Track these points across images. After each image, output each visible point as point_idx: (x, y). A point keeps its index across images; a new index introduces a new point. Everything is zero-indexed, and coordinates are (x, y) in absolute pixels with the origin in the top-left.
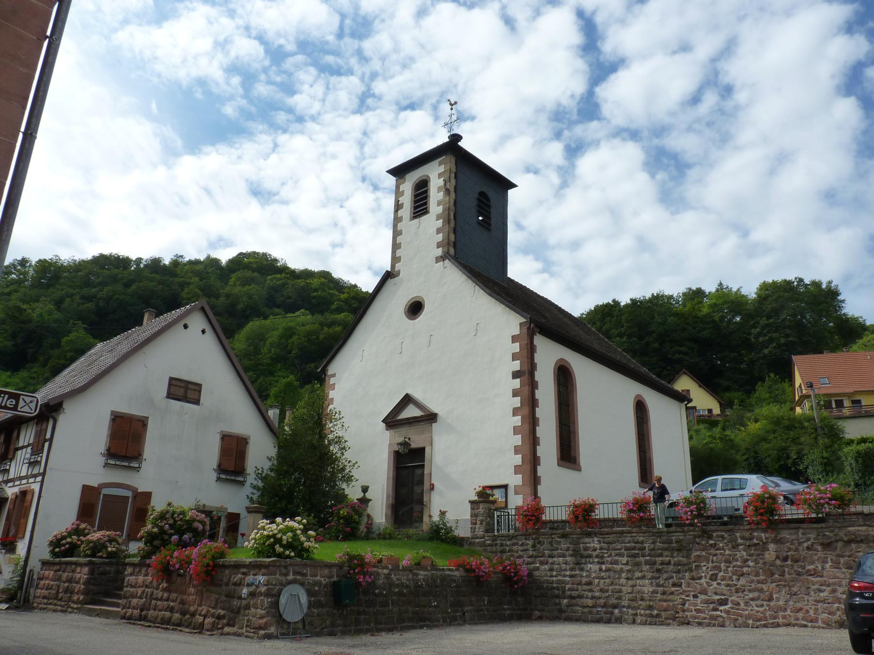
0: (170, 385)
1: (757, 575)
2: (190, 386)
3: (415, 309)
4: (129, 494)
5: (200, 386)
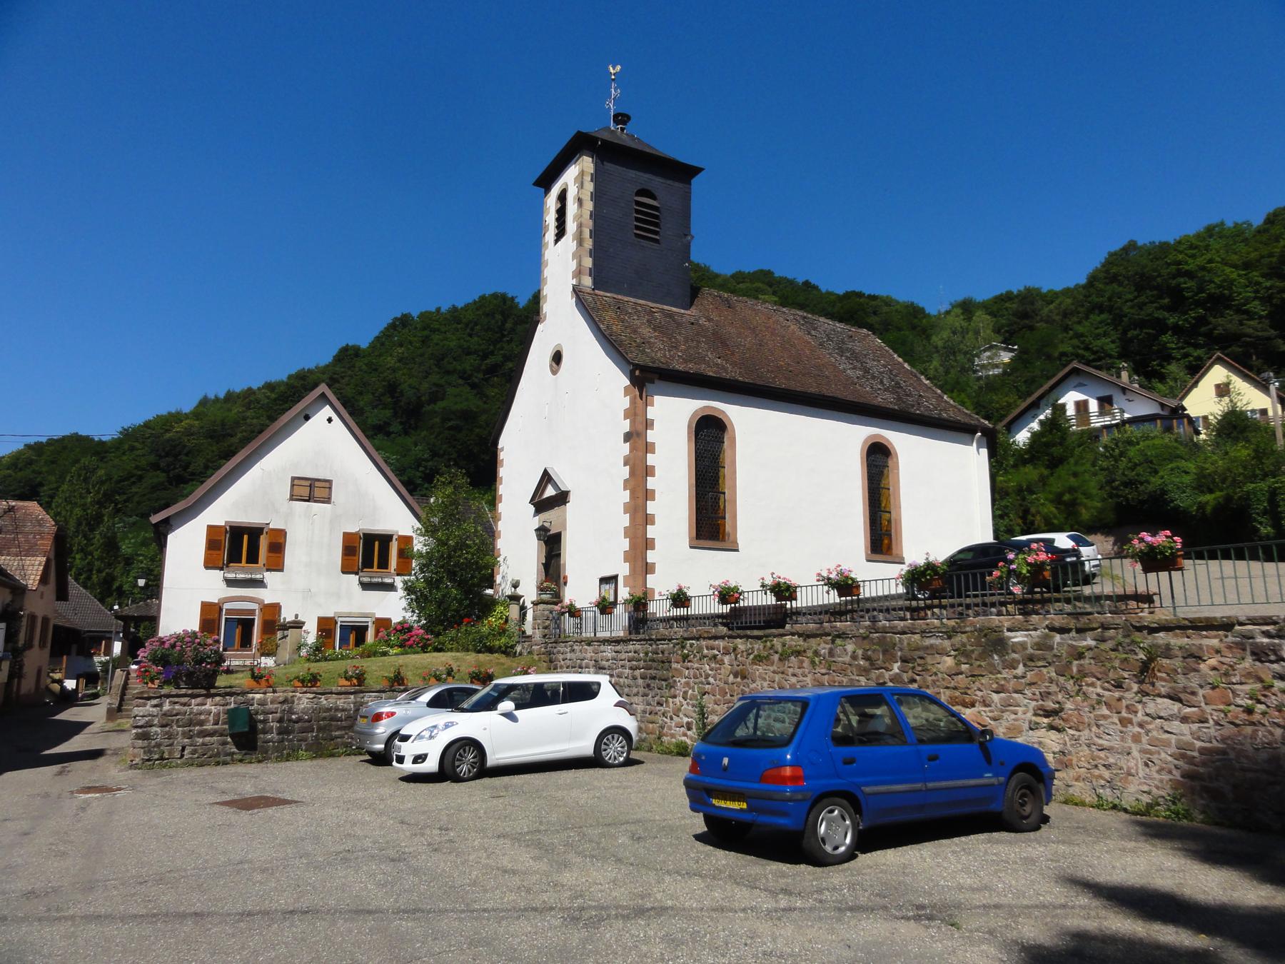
0: (293, 485)
1: (689, 729)
2: (317, 484)
3: (557, 358)
4: (255, 606)
5: (330, 482)
